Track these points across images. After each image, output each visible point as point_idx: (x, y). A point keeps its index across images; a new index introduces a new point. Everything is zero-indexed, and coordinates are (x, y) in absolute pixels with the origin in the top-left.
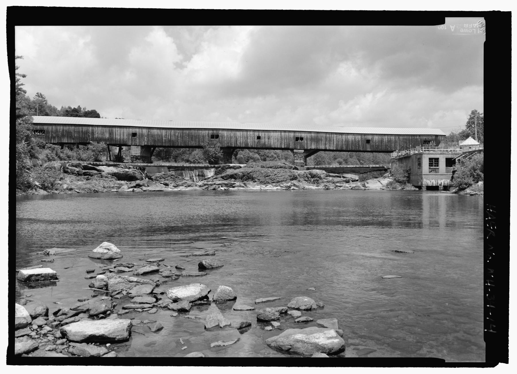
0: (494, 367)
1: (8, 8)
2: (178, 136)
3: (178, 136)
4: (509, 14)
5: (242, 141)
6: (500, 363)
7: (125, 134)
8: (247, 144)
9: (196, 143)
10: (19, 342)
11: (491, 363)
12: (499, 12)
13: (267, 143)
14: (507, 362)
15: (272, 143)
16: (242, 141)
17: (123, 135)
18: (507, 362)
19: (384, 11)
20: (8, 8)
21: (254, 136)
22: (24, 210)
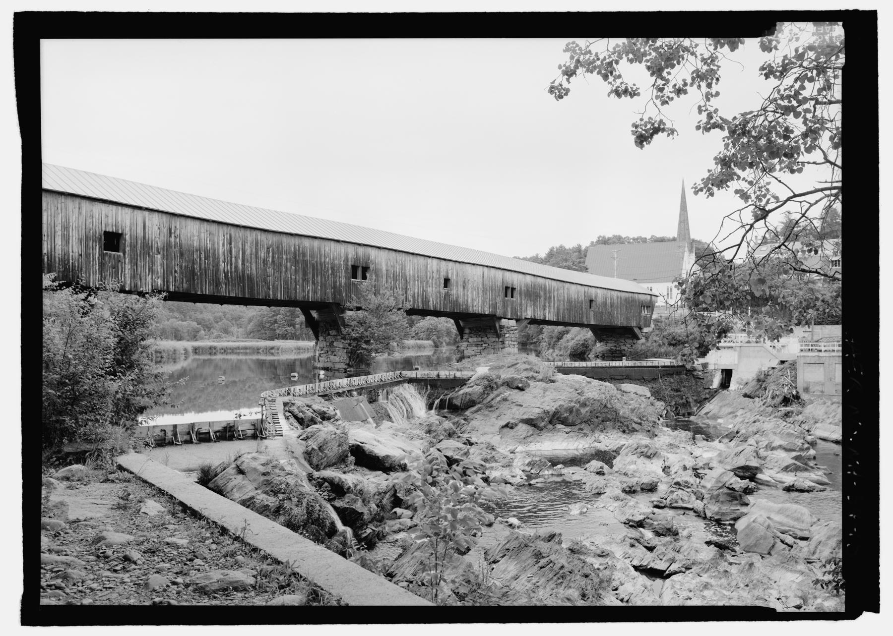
0: (854, 618)
1: (16, 14)
2: (265, 262)
3: (265, 262)
4: (876, 11)
5: (416, 291)
6: (865, 614)
7: (74, 237)
8: (425, 301)
9: (315, 292)
10: (253, 316)
11: (851, 613)
12: (856, 11)
13: (461, 300)
14: (876, 609)
15: (469, 300)
16: (416, 291)
17: (66, 239)
18: (876, 609)
19: (22, 610)
20: (16, 14)
21: (439, 278)
22: (56, 491)
